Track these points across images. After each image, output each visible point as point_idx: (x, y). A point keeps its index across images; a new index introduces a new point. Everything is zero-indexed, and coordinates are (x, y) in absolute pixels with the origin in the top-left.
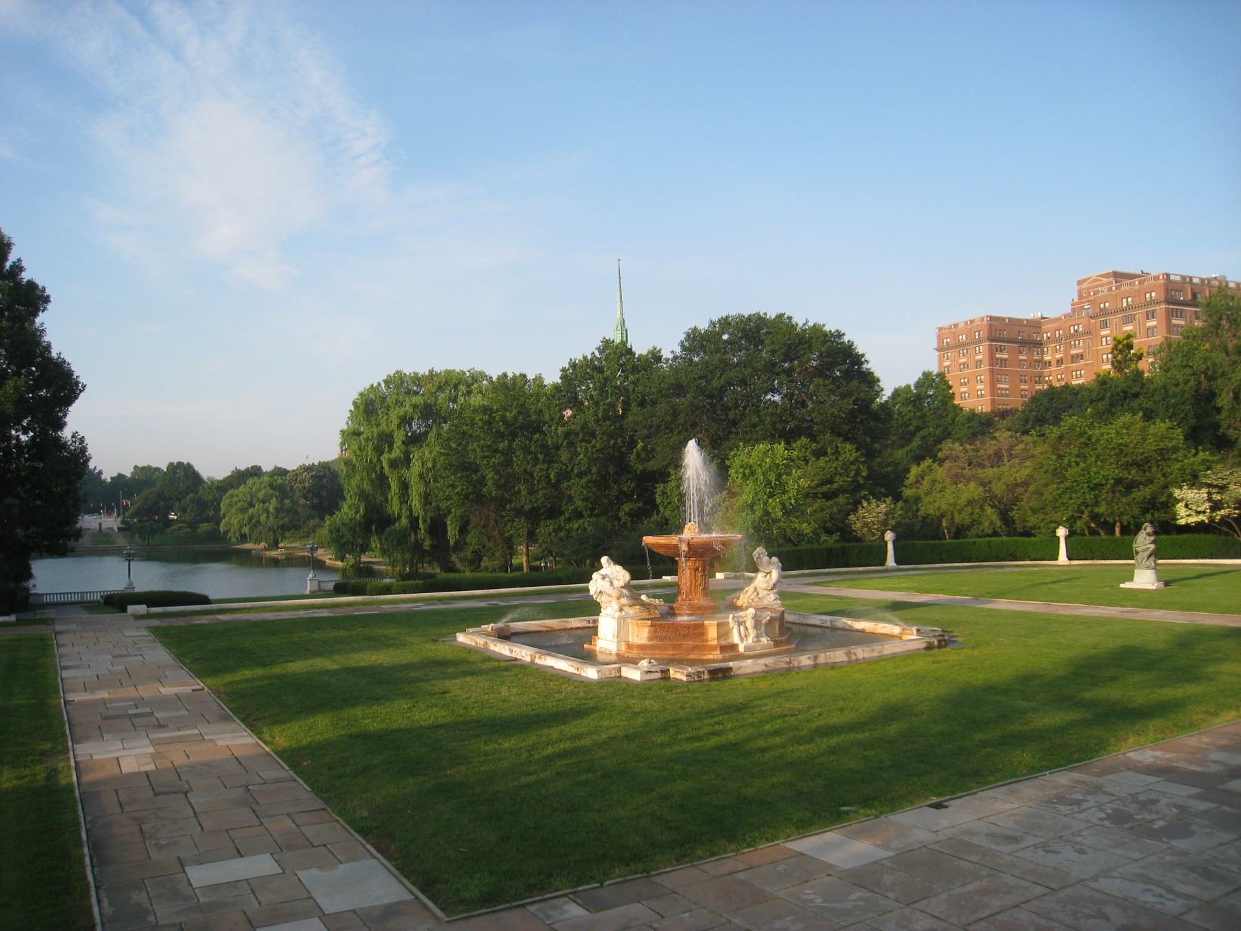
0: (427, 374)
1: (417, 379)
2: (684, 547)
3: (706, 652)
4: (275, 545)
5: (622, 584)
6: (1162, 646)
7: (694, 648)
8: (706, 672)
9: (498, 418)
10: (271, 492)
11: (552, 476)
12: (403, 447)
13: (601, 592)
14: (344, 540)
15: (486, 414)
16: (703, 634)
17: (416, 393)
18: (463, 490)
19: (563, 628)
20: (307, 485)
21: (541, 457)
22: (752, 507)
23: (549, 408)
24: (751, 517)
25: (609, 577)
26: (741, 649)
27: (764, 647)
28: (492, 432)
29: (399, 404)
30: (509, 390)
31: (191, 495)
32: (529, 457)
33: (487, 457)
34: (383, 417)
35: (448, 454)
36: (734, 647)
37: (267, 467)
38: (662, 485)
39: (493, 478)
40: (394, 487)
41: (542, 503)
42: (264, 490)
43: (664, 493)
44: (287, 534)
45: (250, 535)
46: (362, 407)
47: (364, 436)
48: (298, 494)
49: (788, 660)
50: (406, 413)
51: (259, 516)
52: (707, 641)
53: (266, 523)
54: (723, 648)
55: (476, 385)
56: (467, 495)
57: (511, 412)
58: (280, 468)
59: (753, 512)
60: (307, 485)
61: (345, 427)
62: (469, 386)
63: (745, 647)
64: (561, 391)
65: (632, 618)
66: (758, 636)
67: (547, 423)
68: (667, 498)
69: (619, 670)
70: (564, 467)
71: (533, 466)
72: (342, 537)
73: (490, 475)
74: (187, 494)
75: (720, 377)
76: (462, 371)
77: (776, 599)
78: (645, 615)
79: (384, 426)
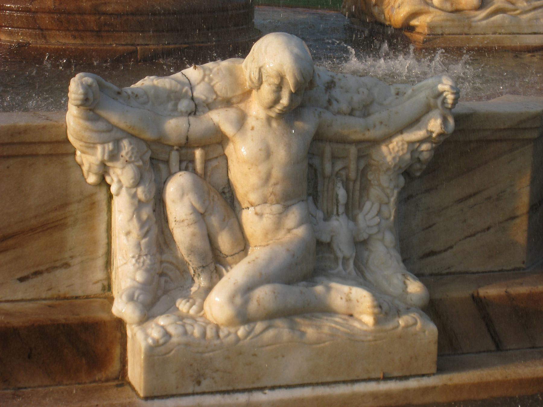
19: (226, 396)
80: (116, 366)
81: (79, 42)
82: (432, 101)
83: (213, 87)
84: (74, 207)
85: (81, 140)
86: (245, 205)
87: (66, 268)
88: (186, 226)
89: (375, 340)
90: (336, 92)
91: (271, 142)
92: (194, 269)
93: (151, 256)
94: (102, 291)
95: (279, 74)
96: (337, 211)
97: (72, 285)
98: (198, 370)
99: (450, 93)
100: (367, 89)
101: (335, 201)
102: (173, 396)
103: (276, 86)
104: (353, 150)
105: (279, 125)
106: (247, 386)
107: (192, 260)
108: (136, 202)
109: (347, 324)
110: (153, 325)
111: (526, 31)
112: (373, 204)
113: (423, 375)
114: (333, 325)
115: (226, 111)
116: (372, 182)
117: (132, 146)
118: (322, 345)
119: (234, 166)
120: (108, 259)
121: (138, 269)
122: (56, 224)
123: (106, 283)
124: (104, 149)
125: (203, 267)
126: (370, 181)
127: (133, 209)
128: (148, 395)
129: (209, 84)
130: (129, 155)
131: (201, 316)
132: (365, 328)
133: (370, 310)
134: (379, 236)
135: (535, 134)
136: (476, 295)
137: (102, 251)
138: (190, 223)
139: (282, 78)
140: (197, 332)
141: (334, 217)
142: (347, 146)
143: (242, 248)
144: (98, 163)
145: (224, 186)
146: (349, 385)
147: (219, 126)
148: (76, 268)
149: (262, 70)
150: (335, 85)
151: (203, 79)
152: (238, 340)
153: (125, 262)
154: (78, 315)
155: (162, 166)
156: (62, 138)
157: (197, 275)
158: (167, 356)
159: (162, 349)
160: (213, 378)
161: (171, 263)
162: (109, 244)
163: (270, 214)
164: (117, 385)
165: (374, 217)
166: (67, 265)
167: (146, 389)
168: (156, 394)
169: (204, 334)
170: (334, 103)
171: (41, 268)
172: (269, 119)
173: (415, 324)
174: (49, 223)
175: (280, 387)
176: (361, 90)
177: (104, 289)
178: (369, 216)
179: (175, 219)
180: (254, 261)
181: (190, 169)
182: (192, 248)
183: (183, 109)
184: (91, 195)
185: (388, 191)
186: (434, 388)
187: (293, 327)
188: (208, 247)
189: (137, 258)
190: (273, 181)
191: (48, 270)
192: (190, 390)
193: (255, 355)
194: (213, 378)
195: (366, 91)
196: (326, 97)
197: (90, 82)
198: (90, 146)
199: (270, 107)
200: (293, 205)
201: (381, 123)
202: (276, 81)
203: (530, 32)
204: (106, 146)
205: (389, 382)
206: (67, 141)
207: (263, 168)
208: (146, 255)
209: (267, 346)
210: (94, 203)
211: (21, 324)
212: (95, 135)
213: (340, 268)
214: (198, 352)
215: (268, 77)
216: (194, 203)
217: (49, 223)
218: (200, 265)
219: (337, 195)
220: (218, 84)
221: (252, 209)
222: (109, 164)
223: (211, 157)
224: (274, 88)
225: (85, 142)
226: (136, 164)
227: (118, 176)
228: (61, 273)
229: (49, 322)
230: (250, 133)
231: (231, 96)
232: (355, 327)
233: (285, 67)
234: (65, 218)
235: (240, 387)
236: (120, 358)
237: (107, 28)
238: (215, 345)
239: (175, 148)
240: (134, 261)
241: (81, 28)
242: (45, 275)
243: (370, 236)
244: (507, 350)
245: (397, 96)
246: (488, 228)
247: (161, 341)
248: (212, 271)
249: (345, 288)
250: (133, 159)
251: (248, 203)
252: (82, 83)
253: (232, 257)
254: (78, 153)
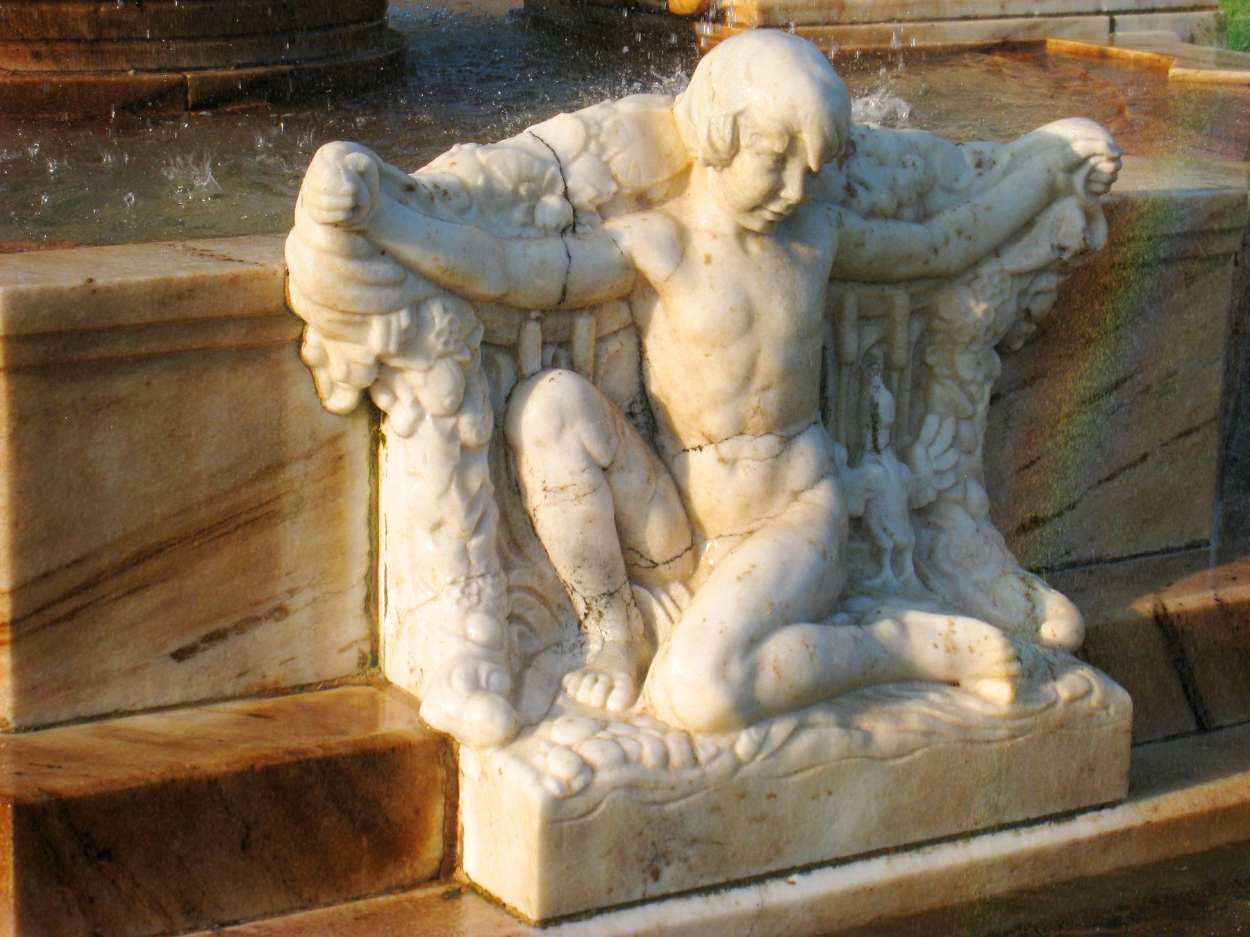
65: (757, 234)
80: (433, 848)
81: (45, 66)
82: (1061, 178)
83: (606, 165)
84: (295, 470)
85: (332, 308)
86: (690, 440)
87: (277, 620)
88: (572, 500)
89: (1013, 737)
90: (858, 164)
91: (755, 290)
92: (587, 600)
93: (493, 576)
94: (358, 666)
95: (787, 129)
96: (875, 441)
97: (293, 659)
98: (653, 844)
99: (1104, 158)
100: (920, 155)
101: (867, 419)
102: (601, 911)
103: (774, 157)
104: (900, 299)
105: (763, 249)
106: (754, 872)
107: (584, 580)
108: (458, 450)
109: (951, 704)
110: (543, 747)
111: (949, 14)
112: (942, 420)
113: (1100, 807)
114: (926, 710)
115: (644, 220)
116: (937, 370)
117: (449, 316)
118: (907, 759)
119: (662, 349)
120: (369, 590)
121: (470, 610)
122: (258, 513)
123: (366, 648)
124: (388, 325)
125: (611, 595)
126: (931, 368)
127: (449, 469)
128: (550, 915)
129: (599, 156)
130: (442, 340)
131: (642, 715)
132: (991, 711)
133: (1001, 669)
134: (957, 495)
135: (1233, 243)
136: (1160, 611)
137: (358, 571)
138: (582, 492)
139: (792, 140)
140: (649, 756)
141: (869, 457)
142: (888, 290)
143: (688, 544)
144: (370, 360)
145: (632, 399)
146: (960, 843)
147: (632, 258)
148: (300, 618)
149: (741, 120)
150: (855, 149)
151: (585, 148)
152: (738, 765)
153: (432, 595)
154: (343, 733)
155: (503, 360)
156: (274, 303)
157: (594, 614)
158: (590, 817)
159: (579, 804)
160: (686, 860)
161: (530, 590)
162: (374, 555)
163: (753, 459)
164: (447, 892)
165: (946, 451)
166: (281, 612)
167: (545, 901)
168: (564, 911)
169: (665, 759)
170: (861, 191)
171: (222, 624)
172: (742, 234)
173: (1089, 692)
174: (241, 514)
175: (821, 865)
176: (909, 158)
177: (362, 663)
178: (937, 449)
179: (544, 485)
180: (748, 573)
181: (563, 362)
182: (584, 551)
183: (551, 222)
184: (335, 439)
185: (973, 388)
186: (1127, 833)
187: (846, 725)
188: (616, 547)
189: (463, 584)
190: (759, 380)
191: (239, 628)
192: (637, 896)
193: (772, 796)
194: (686, 860)
195: (919, 161)
196: (842, 180)
197: (364, 164)
198: (355, 321)
199: (755, 208)
200: (799, 434)
201: (960, 233)
202: (778, 147)
203: (957, 15)
204: (393, 318)
205: (1037, 827)
206: (286, 314)
207: (738, 353)
208: (483, 576)
209: (796, 772)
210: (341, 458)
211: (224, 768)
212: (369, 293)
213: (888, 572)
214: (655, 803)
215: (754, 137)
216: (587, 444)
217: (241, 514)
218: (604, 590)
219: (875, 406)
220: (619, 158)
221: (709, 451)
222: (396, 362)
223: (605, 332)
224: (768, 162)
225: (344, 312)
226: (458, 358)
227: (412, 389)
228: (268, 632)
229: (288, 758)
230: (703, 272)
231: (648, 185)
232: (969, 710)
233: (801, 114)
234: (278, 497)
235: (739, 874)
236: (443, 829)
237: (113, 33)
238: (691, 782)
239: (534, 315)
240: (456, 592)
241: (54, 34)
242: (232, 638)
243: (940, 493)
244: (1221, 728)
245: (980, 170)
246: (1144, 457)
247: (577, 784)
248: (628, 601)
249: (939, 622)
250: (452, 347)
251: (700, 435)
252: (346, 169)
253: (667, 566)
254: (312, 338)
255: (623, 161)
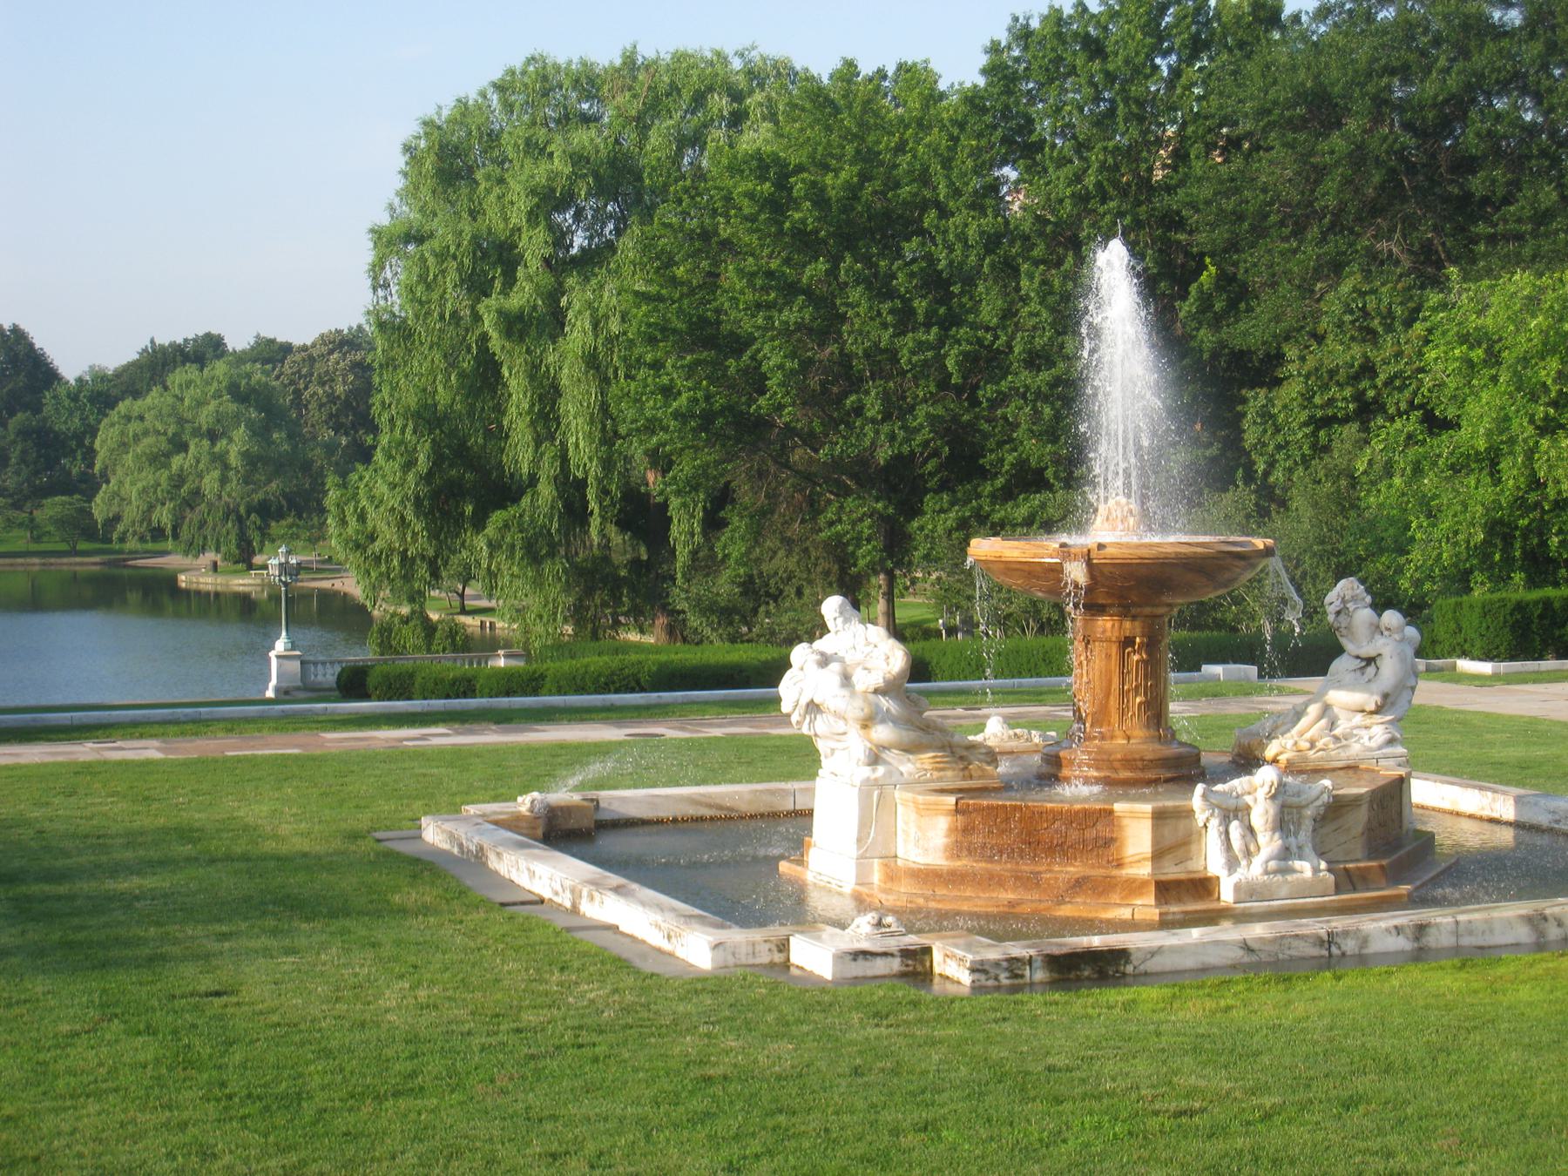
0: (618, 62)
1: (588, 82)
2: (1076, 572)
3: (1115, 898)
4: (245, 557)
5: (877, 680)
6: (1272, 812)
7: (1079, 884)
8: (1038, 963)
9: (799, 188)
10: (233, 407)
11: (950, 364)
12: (547, 280)
13: (813, 708)
14: (378, 546)
15: (762, 178)
16: (1109, 842)
17: (586, 119)
18: (695, 401)
20: (340, 389)
21: (920, 305)
22: (1494, 463)
23: (947, 163)
24: (1486, 493)
25: (841, 660)
26: (1227, 895)
27: (1303, 889)
28: (781, 233)
29: (532, 149)
30: (837, 110)
31: (20, 416)
32: (887, 306)
33: (770, 306)
34: (488, 191)
35: (659, 298)
36: (1203, 886)
37: (238, 341)
38: (1262, 392)
39: (781, 367)
40: (516, 385)
41: (926, 444)
42: (214, 403)
43: (1266, 415)
44: (276, 528)
45: (175, 528)
46: (429, 165)
47: (435, 244)
48: (314, 414)
49: (1323, 933)
50: (553, 176)
51: (201, 477)
52: (1120, 865)
53: (220, 497)
54: (1165, 890)
55: (758, 97)
56: (707, 419)
57: (836, 172)
58: (273, 341)
59: (1496, 479)
60: (340, 389)
61: (384, 220)
62: (737, 96)
63: (1237, 888)
64: (984, 111)
65: (909, 785)
66: (1286, 854)
67: (938, 205)
68: (1278, 430)
69: (784, 946)
70: (989, 336)
71: (894, 336)
72: (372, 538)
73: (773, 357)
74: (12, 413)
75: (1447, 70)
76: (718, 54)
77: (1391, 742)
78: (951, 778)
79: (492, 217)
255: (1246, 787)
